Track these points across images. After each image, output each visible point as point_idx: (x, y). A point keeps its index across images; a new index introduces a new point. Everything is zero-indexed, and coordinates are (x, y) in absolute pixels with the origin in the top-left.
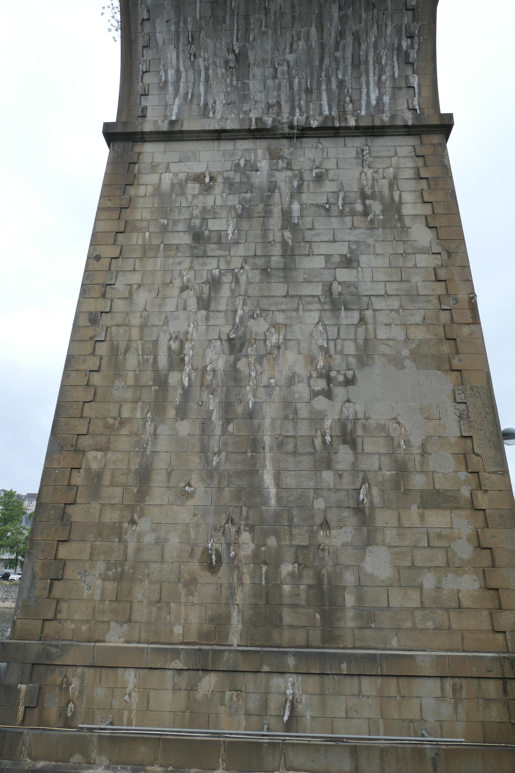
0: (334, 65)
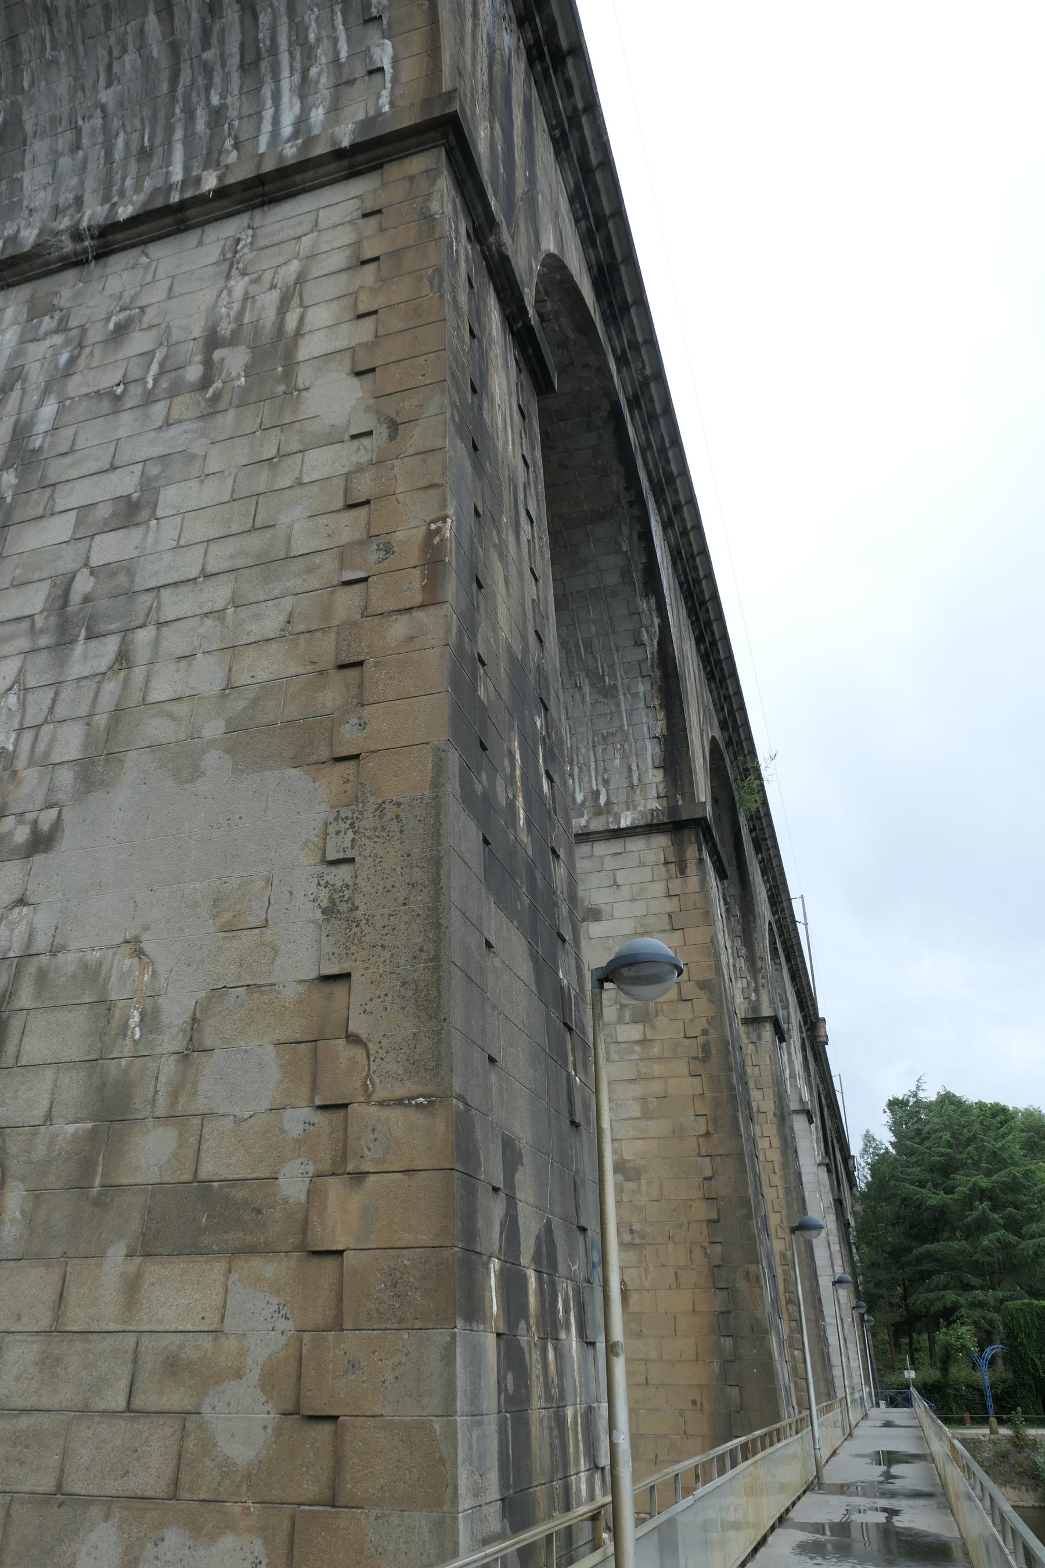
0: (201, 81)
